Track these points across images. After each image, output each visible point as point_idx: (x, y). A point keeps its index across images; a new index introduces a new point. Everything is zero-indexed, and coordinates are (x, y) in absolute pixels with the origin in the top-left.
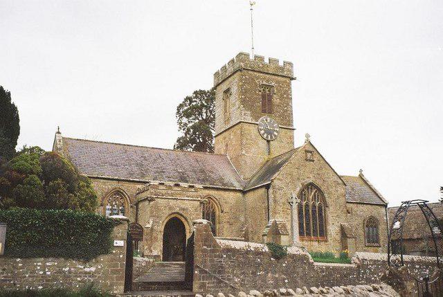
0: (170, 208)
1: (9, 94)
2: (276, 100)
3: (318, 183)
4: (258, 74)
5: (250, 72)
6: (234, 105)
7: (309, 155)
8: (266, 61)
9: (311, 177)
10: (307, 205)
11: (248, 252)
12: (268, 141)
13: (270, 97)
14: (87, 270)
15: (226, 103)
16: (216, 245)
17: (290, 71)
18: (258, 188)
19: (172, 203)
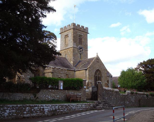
0: (58, 76)
1: (87, 28)
2: (83, 40)
3: (100, 69)
4: (78, 31)
5: (76, 30)
6: (70, 41)
7: (98, 60)
8: (81, 26)
9: (98, 67)
10: (97, 77)
11: (108, 90)
12: (81, 54)
13: (81, 39)
14: (79, 94)
15: (65, 39)
16: (103, 88)
17: (88, 31)
18: (82, 70)
19: (58, 74)
